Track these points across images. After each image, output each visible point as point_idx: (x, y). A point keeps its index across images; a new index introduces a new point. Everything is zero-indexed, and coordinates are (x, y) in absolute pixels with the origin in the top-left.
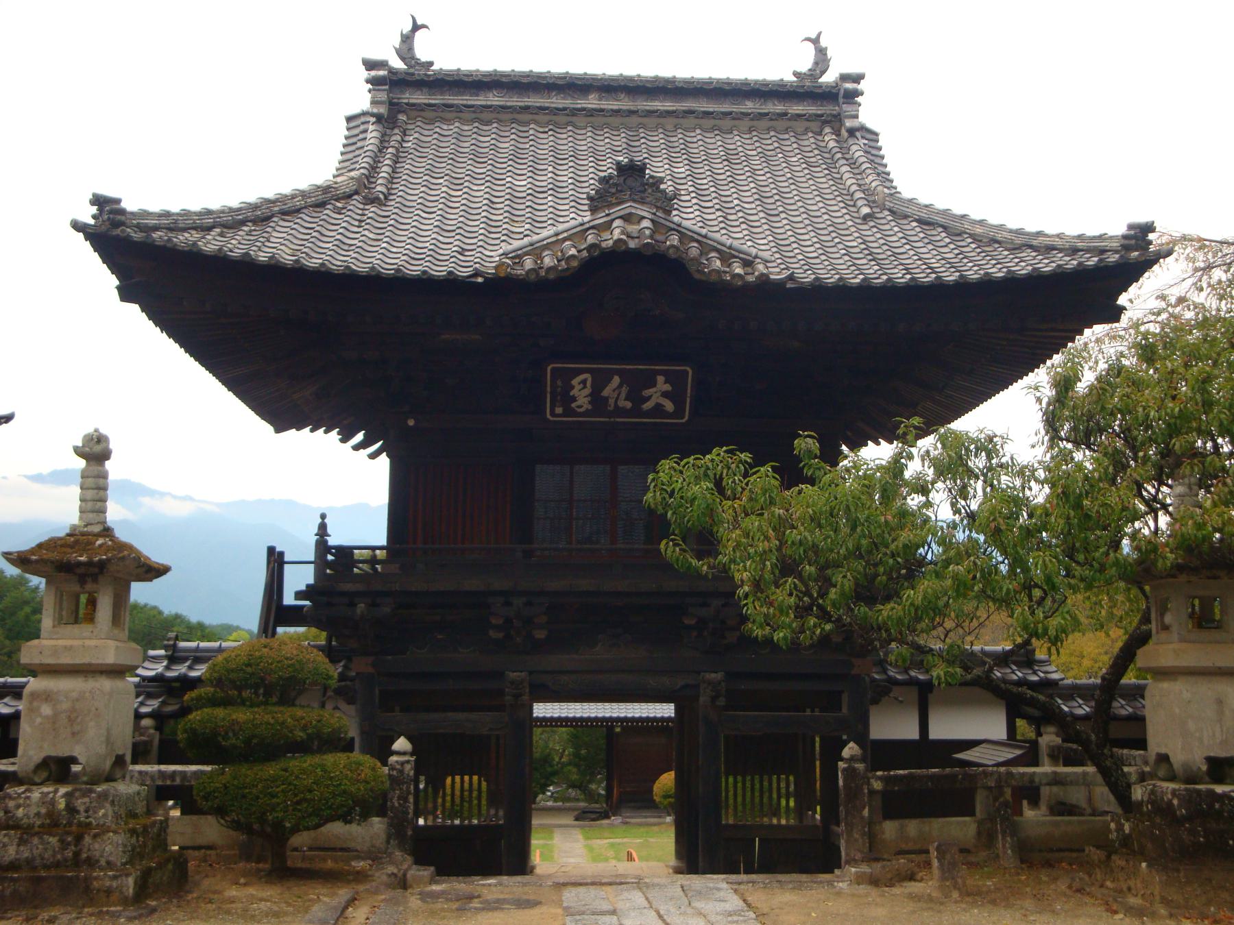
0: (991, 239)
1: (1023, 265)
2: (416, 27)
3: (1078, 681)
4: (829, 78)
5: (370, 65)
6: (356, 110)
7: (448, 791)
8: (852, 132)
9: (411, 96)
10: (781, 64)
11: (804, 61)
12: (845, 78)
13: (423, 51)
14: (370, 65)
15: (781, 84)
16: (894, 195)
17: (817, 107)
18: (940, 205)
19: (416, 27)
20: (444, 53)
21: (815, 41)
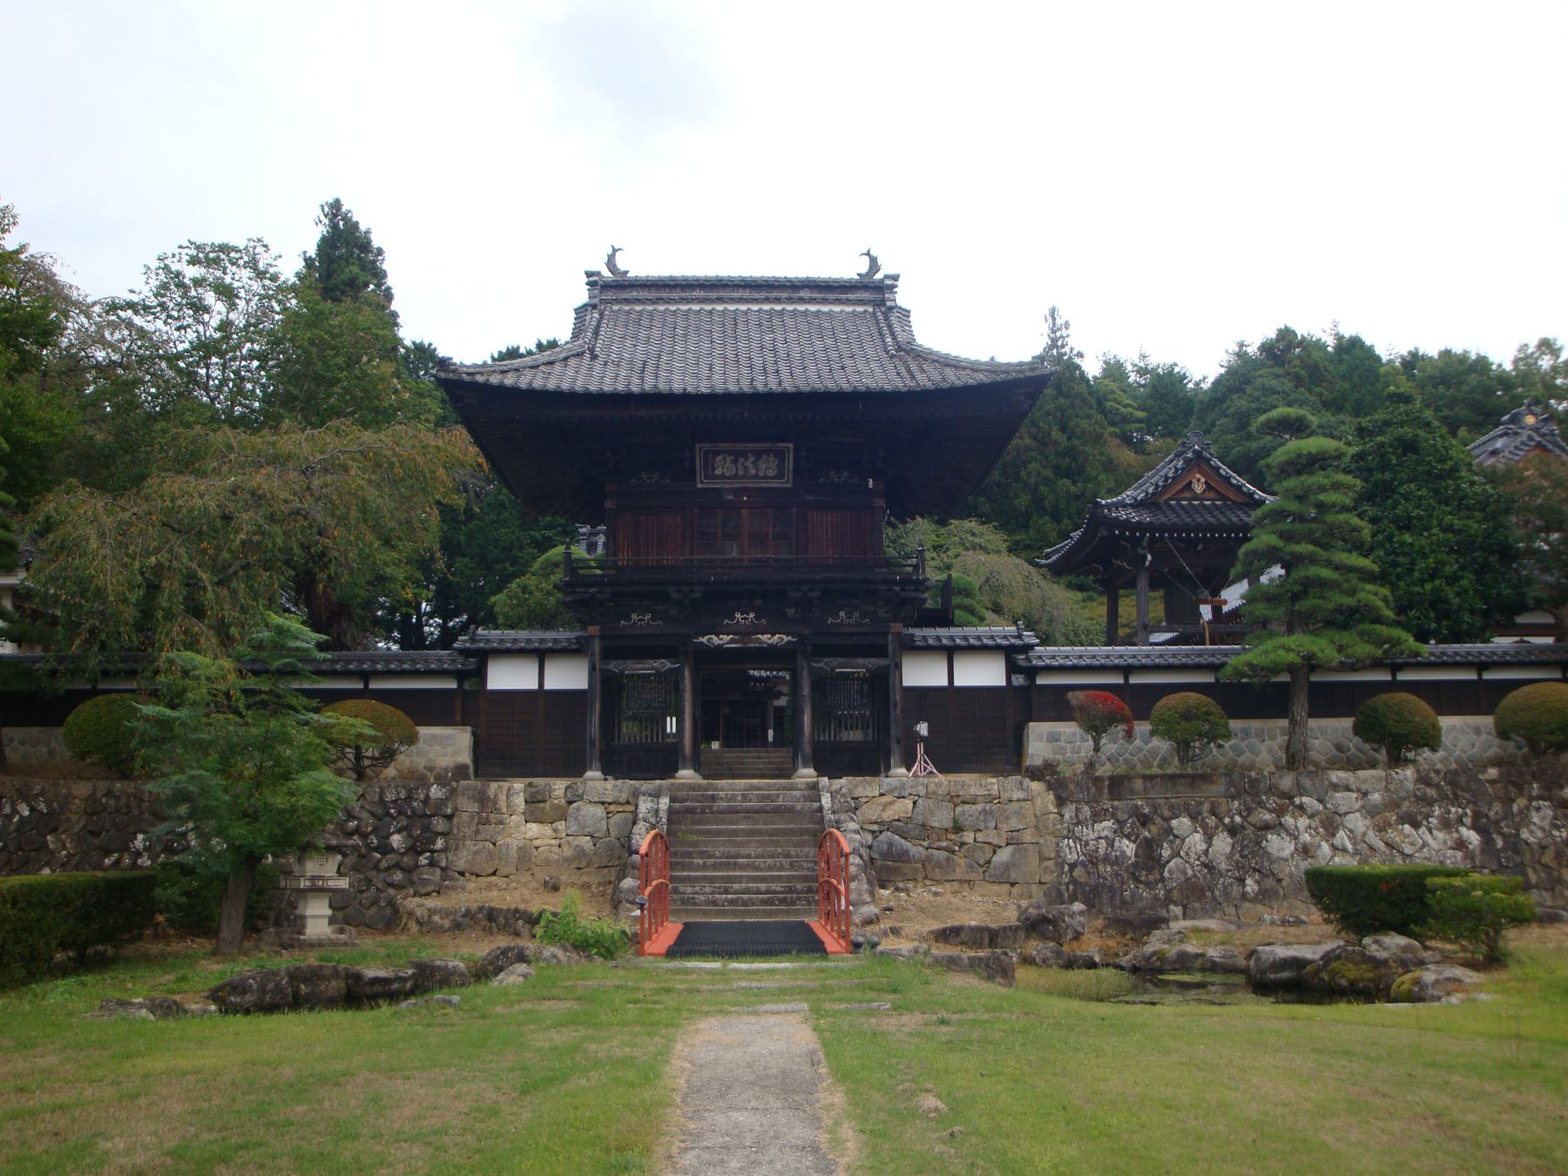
0: (974, 367)
1: (953, 378)
2: (615, 251)
3: (715, 965)
4: (879, 276)
5: (589, 274)
6: (580, 303)
7: (1478, 442)
8: (891, 309)
9: (613, 291)
10: (850, 268)
11: (864, 266)
12: (886, 277)
13: (622, 263)
14: (589, 274)
15: (850, 281)
16: (911, 341)
17: (873, 292)
18: (954, 353)
19: (615, 251)
20: (637, 266)
21: (868, 254)
